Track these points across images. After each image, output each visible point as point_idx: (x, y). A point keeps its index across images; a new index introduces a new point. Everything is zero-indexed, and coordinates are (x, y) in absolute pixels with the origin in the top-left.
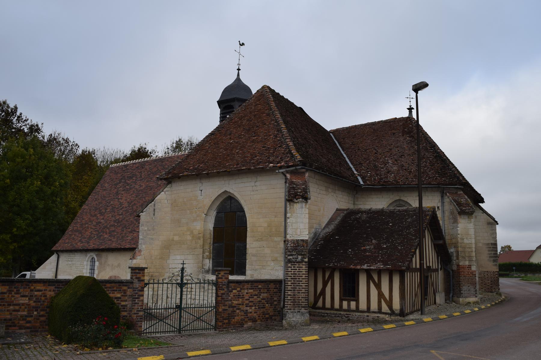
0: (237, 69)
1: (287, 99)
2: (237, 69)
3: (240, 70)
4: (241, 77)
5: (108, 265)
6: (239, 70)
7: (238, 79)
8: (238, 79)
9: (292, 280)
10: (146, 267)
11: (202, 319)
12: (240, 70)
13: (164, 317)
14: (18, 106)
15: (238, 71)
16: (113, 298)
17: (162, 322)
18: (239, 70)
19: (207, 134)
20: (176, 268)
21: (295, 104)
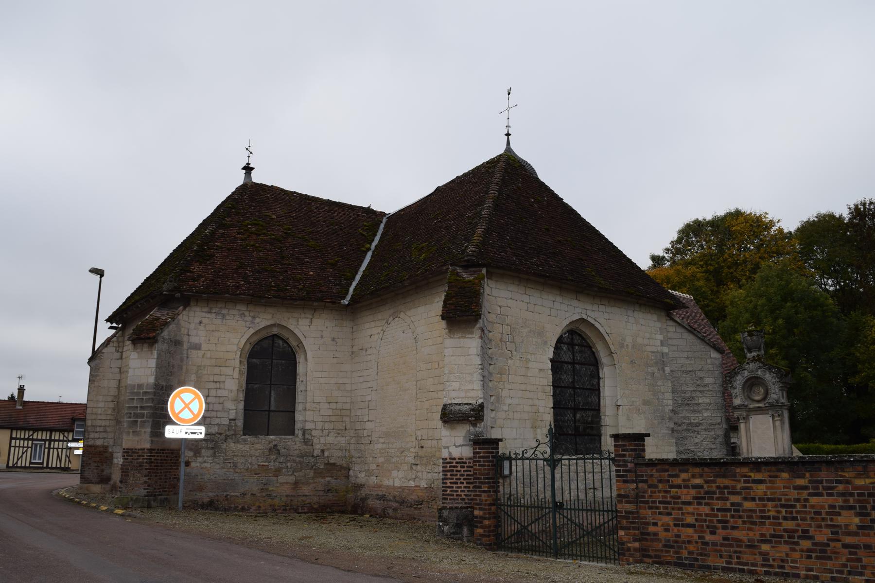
0: (506, 135)
1: (204, 220)
2: (506, 135)
3: (510, 135)
4: (512, 146)
5: (703, 469)
6: (508, 135)
7: (508, 148)
8: (508, 148)
9: (662, 505)
10: (500, 438)
11: (611, 551)
12: (510, 135)
13: (542, 520)
14: (89, 269)
15: (506, 137)
16: (135, 385)
17: (523, 524)
18: (508, 135)
19: (157, 267)
20: (213, 382)
21: (441, 185)
